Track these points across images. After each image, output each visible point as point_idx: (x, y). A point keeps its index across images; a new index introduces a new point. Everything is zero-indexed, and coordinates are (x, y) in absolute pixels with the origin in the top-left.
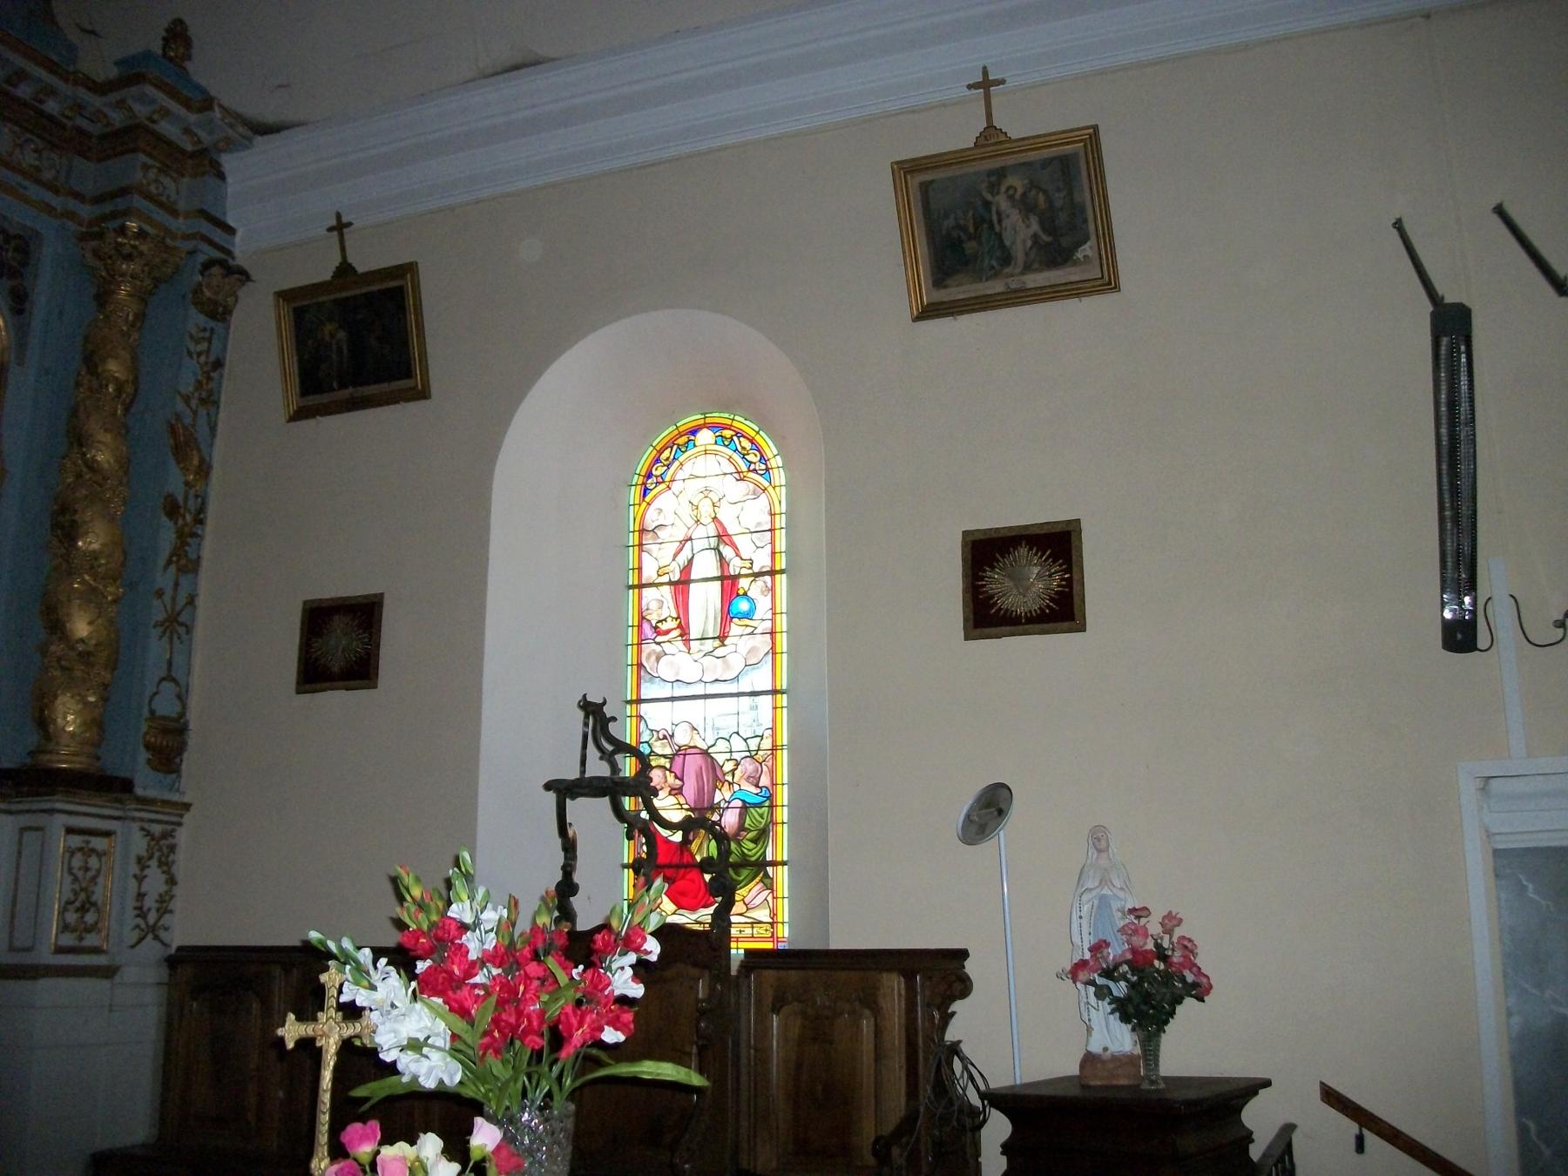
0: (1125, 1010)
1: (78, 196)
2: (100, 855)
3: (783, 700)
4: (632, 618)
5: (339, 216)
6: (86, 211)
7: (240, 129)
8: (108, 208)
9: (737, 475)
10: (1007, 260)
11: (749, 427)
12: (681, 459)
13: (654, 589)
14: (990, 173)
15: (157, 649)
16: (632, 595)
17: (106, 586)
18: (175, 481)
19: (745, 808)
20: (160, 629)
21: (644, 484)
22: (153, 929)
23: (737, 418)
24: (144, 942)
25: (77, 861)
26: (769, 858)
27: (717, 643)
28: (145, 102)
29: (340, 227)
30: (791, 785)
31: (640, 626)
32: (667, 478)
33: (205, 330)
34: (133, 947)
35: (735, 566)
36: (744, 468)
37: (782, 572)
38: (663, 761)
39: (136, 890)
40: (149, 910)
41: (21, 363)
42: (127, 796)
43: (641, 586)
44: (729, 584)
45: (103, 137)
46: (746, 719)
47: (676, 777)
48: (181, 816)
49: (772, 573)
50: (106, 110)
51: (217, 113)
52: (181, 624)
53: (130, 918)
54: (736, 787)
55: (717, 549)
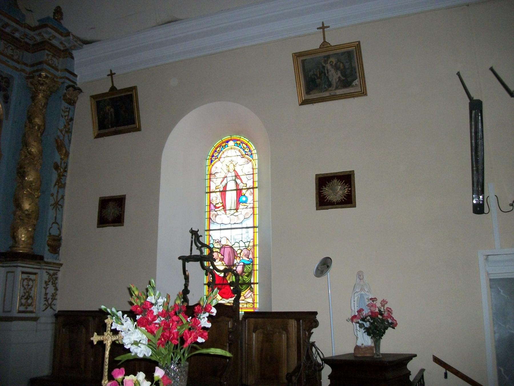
0: (369, 332)
1: (26, 64)
2: (33, 281)
3: (257, 230)
4: (207, 203)
5: (111, 71)
6: (28, 69)
7: (79, 42)
8: (35, 68)
9: (241, 156)
10: (330, 85)
11: (246, 140)
12: (223, 151)
13: (214, 193)
14: (325, 57)
15: (51, 213)
16: (207, 195)
17: (35, 192)
18: (57, 158)
19: (244, 265)
20: (53, 207)
21: (211, 159)
22: (50, 305)
23: (242, 137)
24: (47, 309)
25: (25, 283)
26: (252, 282)
27: (235, 211)
28: (48, 34)
29: (111, 75)
30: (259, 257)
31: (210, 206)
32: (219, 157)
33: (67, 108)
34: (43, 311)
35: (241, 186)
36: (244, 154)
37: (256, 188)
38: (217, 250)
39: (45, 292)
40: (49, 299)
41: (7, 119)
42: (42, 261)
43: (210, 192)
44: (239, 192)
45: (34, 45)
46: (245, 236)
47: (222, 255)
48: (59, 268)
49: (253, 188)
50: (35, 36)
51: (71, 37)
52: (59, 205)
53: (43, 301)
54: (241, 258)
55: (235, 180)
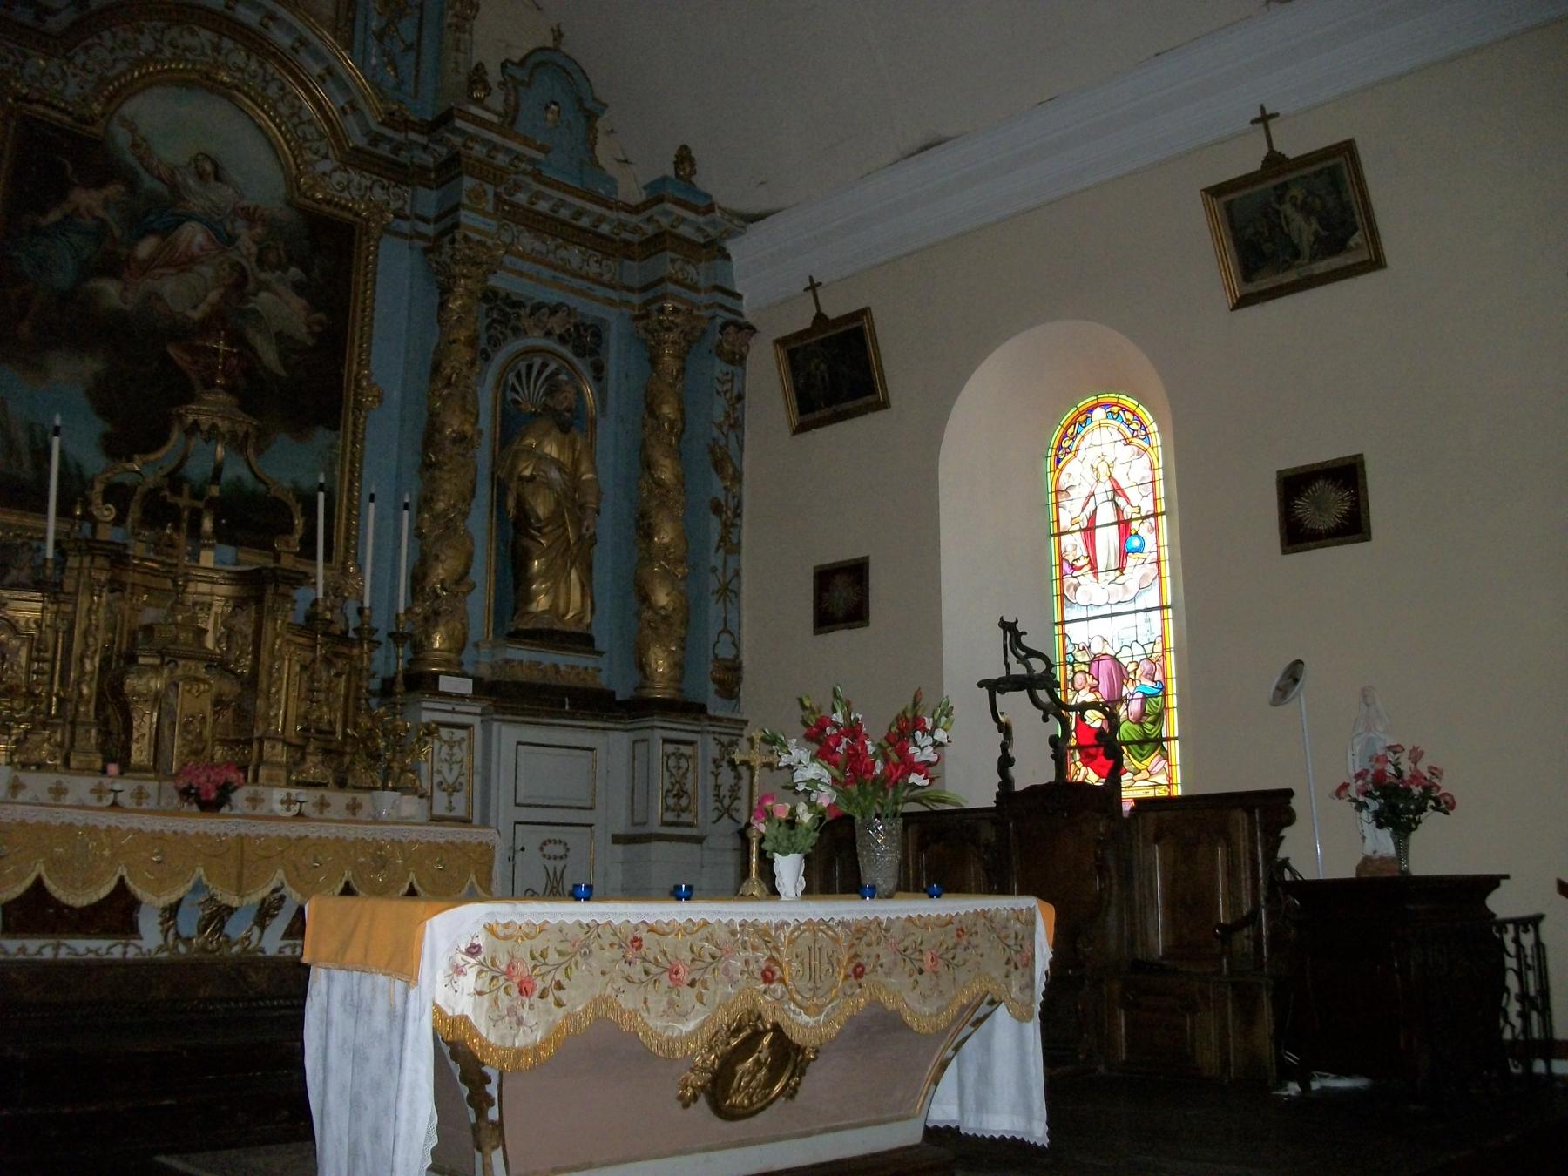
0: (1380, 820)
1: (630, 289)
2: (688, 758)
3: (1169, 613)
4: (1055, 560)
5: (811, 279)
6: (636, 299)
7: (736, 222)
8: (650, 294)
9: (1124, 442)
10: (1297, 254)
11: (1130, 403)
12: (1082, 433)
13: (1069, 536)
14: (1275, 188)
15: (714, 609)
16: (1054, 541)
17: (676, 569)
18: (717, 486)
19: (1145, 697)
20: (716, 596)
21: (1057, 455)
22: (728, 810)
23: (1121, 396)
24: (721, 820)
25: (672, 763)
26: (1164, 735)
27: (1118, 573)
28: (667, 215)
29: (813, 287)
30: (1178, 678)
31: (1061, 565)
32: (1074, 449)
33: (727, 374)
34: (714, 822)
35: (1128, 512)
36: (1130, 436)
37: (1162, 514)
38: (1083, 667)
39: (714, 783)
40: (724, 797)
41: (604, 414)
42: (701, 717)
43: (1060, 534)
44: (1123, 526)
45: (640, 244)
46: (1142, 630)
47: (1094, 678)
48: (742, 729)
49: (1155, 515)
50: (641, 225)
51: (718, 214)
52: (732, 591)
53: (712, 804)
54: (1138, 683)
55: (1113, 500)
